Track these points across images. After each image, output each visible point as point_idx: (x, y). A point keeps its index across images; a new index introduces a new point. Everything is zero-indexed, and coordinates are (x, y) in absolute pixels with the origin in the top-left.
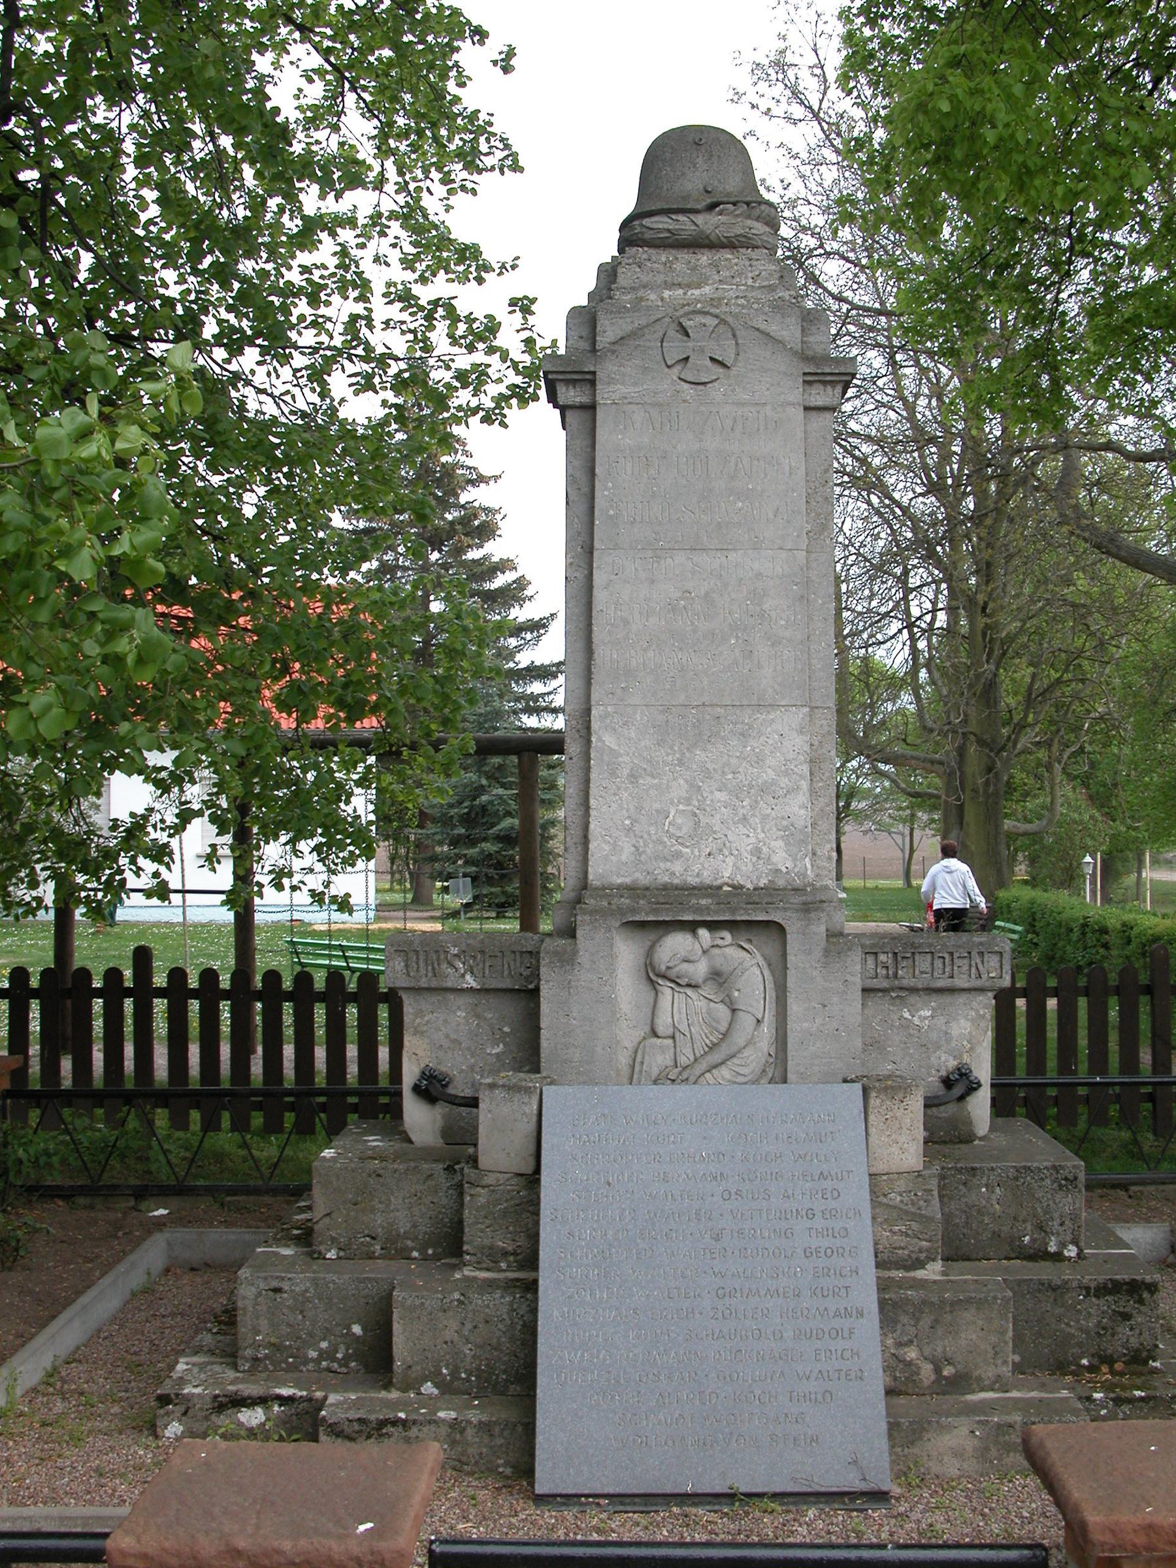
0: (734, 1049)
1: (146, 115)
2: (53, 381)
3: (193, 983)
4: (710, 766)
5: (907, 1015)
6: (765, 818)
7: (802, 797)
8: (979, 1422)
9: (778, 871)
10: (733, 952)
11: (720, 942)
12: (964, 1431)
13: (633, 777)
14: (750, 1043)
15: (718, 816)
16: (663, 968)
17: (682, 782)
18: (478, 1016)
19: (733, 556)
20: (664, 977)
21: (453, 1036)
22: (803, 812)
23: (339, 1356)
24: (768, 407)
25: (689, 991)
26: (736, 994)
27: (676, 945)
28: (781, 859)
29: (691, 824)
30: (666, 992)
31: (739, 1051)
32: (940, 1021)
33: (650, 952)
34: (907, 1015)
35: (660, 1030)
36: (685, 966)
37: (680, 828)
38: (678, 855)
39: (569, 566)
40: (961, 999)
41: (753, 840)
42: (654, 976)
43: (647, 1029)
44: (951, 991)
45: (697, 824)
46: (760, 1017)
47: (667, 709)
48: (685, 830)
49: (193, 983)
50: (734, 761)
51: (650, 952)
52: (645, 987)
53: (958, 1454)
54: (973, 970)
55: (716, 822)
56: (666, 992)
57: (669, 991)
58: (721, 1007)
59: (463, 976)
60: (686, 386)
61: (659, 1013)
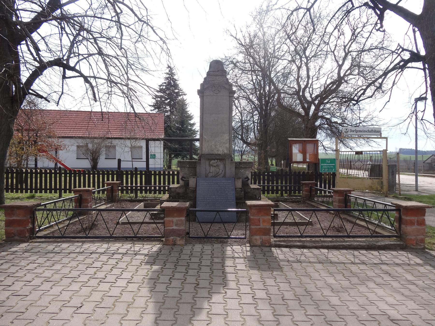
7: (228, 144)
10: (220, 163)
13: (208, 141)
27: (213, 161)
28: (226, 152)
42: (210, 165)
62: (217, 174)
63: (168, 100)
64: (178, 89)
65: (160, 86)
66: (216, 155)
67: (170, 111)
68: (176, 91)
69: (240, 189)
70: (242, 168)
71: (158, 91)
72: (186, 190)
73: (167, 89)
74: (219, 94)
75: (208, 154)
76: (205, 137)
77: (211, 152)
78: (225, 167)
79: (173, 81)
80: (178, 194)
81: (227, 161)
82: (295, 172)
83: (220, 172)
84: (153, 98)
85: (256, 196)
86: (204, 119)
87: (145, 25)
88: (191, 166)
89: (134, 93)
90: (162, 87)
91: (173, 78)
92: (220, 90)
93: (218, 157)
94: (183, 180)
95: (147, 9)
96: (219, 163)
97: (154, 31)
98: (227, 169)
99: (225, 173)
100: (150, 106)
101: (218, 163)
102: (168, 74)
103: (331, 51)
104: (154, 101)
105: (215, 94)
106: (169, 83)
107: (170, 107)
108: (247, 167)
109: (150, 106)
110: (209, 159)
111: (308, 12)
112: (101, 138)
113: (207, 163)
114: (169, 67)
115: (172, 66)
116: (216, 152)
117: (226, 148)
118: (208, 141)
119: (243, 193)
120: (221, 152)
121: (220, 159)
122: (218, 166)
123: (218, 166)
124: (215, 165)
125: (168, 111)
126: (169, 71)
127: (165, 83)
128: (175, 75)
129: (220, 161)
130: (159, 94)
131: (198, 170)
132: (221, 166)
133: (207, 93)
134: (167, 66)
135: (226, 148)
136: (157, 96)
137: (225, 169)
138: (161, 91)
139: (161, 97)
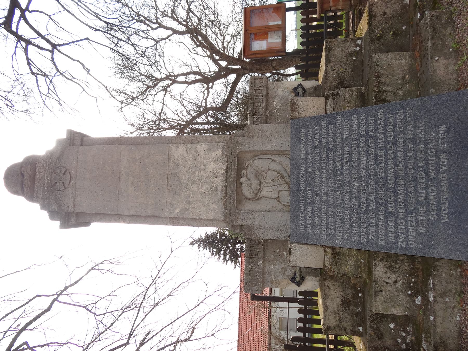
3: (302, 316)
4: (187, 177)
5: (275, 111)
6: (205, 159)
7: (198, 146)
8: (431, 58)
9: (222, 155)
10: (250, 169)
12: (435, 64)
13: (189, 203)
15: (204, 175)
17: (192, 187)
18: (273, 261)
19: (122, 169)
20: (256, 195)
21: (280, 270)
22: (203, 146)
23: (404, 334)
24: (79, 157)
25: (262, 186)
26: (263, 169)
27: (245, 190)
28: (218, 153)
29: (206, 183)
30: (263, 194)
32: (278, 99)
33: (249, 199)
34: (275, 111)
35: (276, 196)
37: (207, 188)
38: (216, 188)
39: (124, 222)
40: (270, 91)
41: (212, 163)
42: (257, 198)
43: (276, 200)
44: (267, 95)
45: (206, 182)
46: (271, 160)
47: (168, 191)
48: (207, 186)
49: (302, 316)
50: (186, 169)
51: (249, 199)
53: (447, 66)
54: (260, 88)
55: (205, 175)
56: (263, 194)
57: (262, 193)
59: (258, 266)
60: (71, 183)
61: (270, 196)
62: (282, 177)
63: (229, 245)
64: (217, 234)
65: (213, 255)
66: (226, 180)
67: (241, 244)
68: (219, 236)
69: (330, 101)
70: (267, 108)
71: (219, 257)
72: (332, 277)
73: (215, 247)
74: (73, 173)
75: (225, 204)
76: (178, 211)
77: (220, 194)
78: (263, 153)
79: (208, 240)
80: (345, 303)
81: (246, 148)
82: (302, 44)
83: (278, 167)
84: (227, 263)
85: (351, 55)
86: (132, 213)
87: (60, 299)
88: (261, 254)
89: (150, 335)
90: (214, 253)
91: (205, 238)
92: (63, 170)
93: (233, 174)
94: (303, 279)
95: (37, 296)
96: (249, 172)
97: (74, 284)
98: (268, 147)
99: (280, 153)
100: (235, 267)
101: (251, 176)
102: (199, 245)
103: (156, 44)
104: (229, 262)
105: (73, 182)
106: (209, 244)
107: (237, 244)
108: (264, 92)
109: (235, 267)
110: (239, 202)
111: (58, 48)
112: (270, 336)
113: (248, 206)
114: (192, 243)
115: (192, 240)
116: (221, 179)
117: (209, 150)
118: (189, 203)
119: (341, 91)
120: (221, 165)
121: (239, 168)
122: (258, 175)
123: (258, 175)
124: (255, 183)
125: (241, 247)
126: (197, 243)
127: (209, 249)
128: (201, 237)
129: (246, 169)
130: (222, 256)
131: (270, 236)
132: (261, 164)
133: (84, 205)
134: (192, 246)
135: (209, 150)
136: (225, 259)
137: (267, 153)
138: (218, 253)
139: (225, 254)
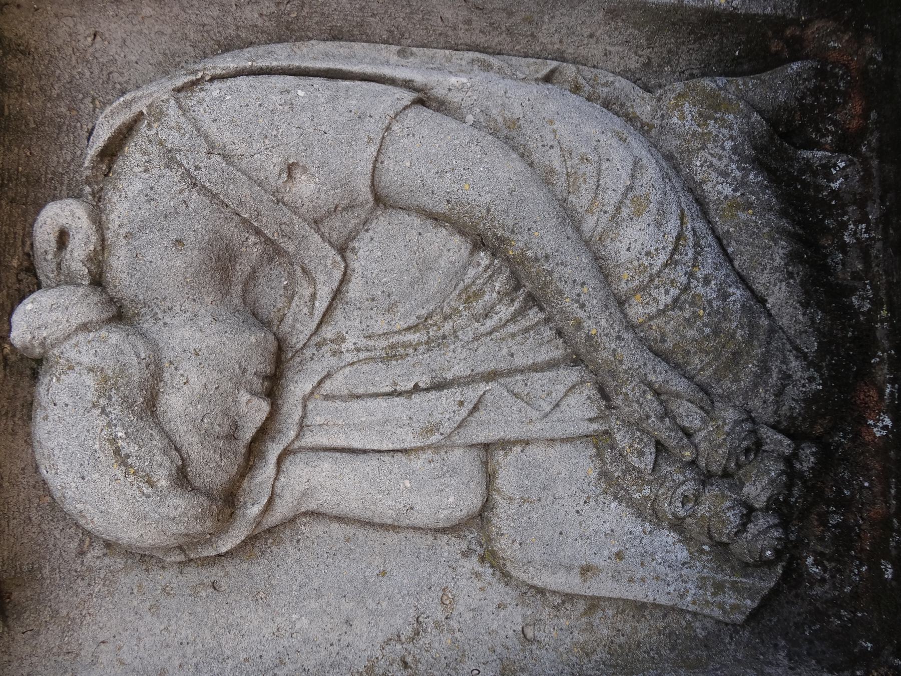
0: (537, 204)
1: (792, 167)
2: (678, 106)
10: (135, 187)
11: (77, 254)
14: (508, 135)
16: (180, 505)
20: (228, 501)
25: (298, 387)
26: (305, 188)
30: (309, 481)
31: (546, 179)
36: (175, 403)
43: (450, 547)
46: (408, 97)
52: (289, 564)
56: (309, 481)
57: (298, 475)
58: (365, 255)
61: (386, 507)
